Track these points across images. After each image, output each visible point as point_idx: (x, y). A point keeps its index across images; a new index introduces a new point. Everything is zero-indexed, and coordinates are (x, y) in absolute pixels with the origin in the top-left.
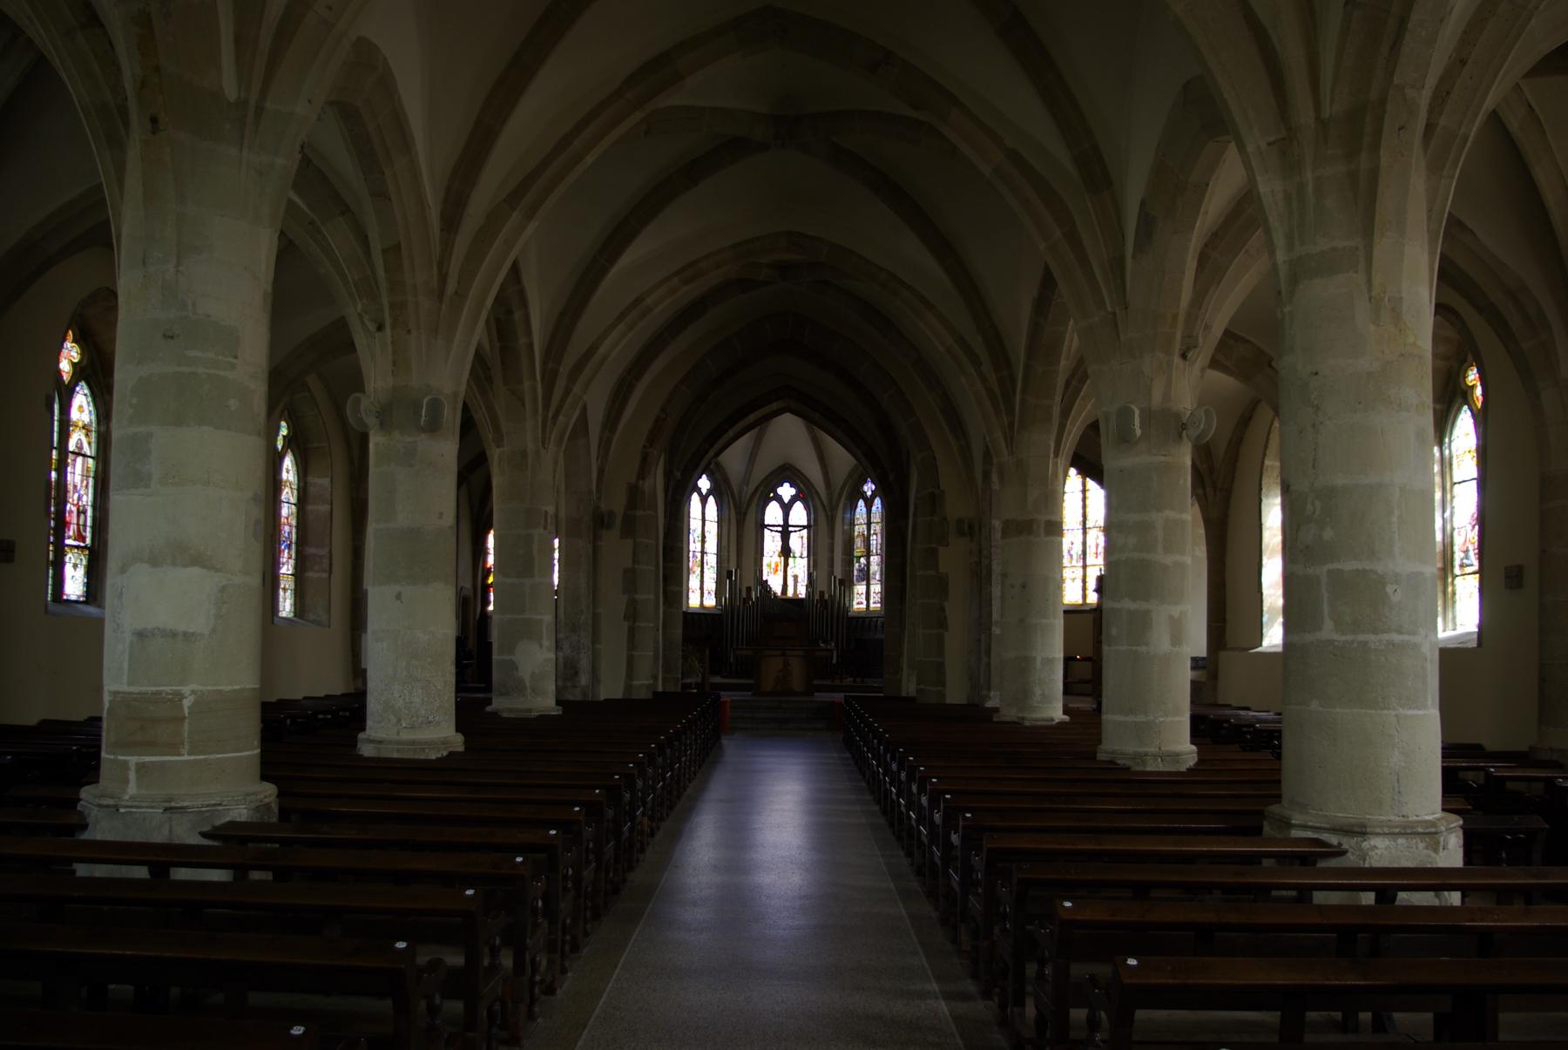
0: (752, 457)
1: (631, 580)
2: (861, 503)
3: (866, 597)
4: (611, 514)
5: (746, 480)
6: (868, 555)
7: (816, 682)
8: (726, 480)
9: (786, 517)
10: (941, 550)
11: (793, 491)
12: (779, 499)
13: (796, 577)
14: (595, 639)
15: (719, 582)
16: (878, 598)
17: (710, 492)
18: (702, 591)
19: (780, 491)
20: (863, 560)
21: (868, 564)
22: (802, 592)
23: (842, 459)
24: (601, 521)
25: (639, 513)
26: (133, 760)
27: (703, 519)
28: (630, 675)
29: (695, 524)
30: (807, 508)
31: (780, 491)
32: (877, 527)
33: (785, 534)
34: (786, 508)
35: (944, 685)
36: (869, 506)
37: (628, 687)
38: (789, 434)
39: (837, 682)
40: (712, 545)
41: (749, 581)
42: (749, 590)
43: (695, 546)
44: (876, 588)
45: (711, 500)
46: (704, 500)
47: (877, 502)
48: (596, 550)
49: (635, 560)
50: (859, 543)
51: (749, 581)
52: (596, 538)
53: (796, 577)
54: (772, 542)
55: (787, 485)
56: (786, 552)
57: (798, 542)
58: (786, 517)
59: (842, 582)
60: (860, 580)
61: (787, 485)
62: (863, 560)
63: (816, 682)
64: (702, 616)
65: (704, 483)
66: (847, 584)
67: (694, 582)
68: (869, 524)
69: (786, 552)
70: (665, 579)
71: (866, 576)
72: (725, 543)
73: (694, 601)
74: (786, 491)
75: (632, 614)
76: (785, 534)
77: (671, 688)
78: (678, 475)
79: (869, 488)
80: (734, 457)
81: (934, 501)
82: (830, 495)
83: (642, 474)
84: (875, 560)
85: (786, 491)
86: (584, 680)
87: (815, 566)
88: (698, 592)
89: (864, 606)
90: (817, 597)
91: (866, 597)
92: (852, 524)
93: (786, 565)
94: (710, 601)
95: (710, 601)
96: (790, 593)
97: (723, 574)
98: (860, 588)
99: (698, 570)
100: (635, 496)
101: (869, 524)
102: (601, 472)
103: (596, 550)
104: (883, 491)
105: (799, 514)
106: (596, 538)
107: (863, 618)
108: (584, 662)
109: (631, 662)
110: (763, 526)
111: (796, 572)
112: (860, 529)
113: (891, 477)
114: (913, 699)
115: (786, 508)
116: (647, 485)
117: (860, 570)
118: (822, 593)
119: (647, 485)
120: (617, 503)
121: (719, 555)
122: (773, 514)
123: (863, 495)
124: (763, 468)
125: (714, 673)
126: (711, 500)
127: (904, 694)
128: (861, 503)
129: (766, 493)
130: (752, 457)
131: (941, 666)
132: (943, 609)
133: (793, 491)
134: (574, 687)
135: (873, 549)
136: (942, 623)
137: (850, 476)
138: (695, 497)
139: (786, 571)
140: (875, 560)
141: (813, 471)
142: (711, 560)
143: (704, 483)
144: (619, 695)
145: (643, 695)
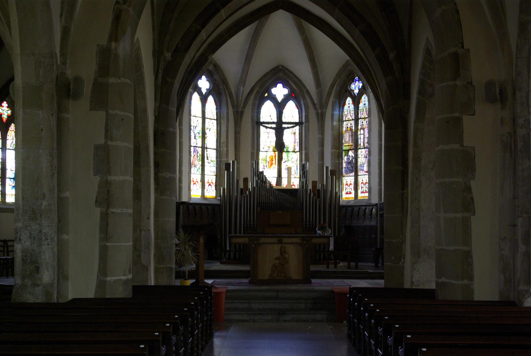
0: (248, 59)
1: (103, 159)
2: (349, 100)
3: (356, 187)
4: (78, 81)
5: (243, 81)
6: (356, 149)
7: (313, 268)
8: (225, 82)
9: (279, 113)
10: (467, 120)
11: (286, 91)
12: (273, 99)
13: (289, 170)
14: (61, 226)
15: (219, 175)
16: (366, 188)
17: (210, 92)
18: (201, 183)
19: (274, 91)
20: (351, 153)
21: (356, 157)
22: (296, 183)
23: (332, 55)
24: (66, 90)
25: (112, 80)
26: (228, 235)
27: (202, 115)
28: (103, 270)
29: (196, 122)
30: (299, 106)
31: (274, 91)
32: (363, 123)
33: (279, 129)
34: (280, 107)
35: (471, 278)
36: (356, 101)
37: (101, 284)
38: (281, 36)
39: (332, 268)
40: (211, 141)
41: (246, 172)
42: (246, 180)
43: (196, 142)
44: (363, 178)
45: (211, 99)
46: (204, 99)
47: (364, 99)
48: (60, 122)
49: (108, 135)
50: (347, 139)
51: (246, 172)
52: (61, 109)
53: (289, 170)
54: (267, 138)
55: (280, 86)
56: (280, 147)
57: (291, 138)
58: (279, 113)
59: (333, 173)
60: (349, 171)
61: (280, 86)
62: (351, 153)
63: (313, 268)
64: (202, 208)
65: (204, 84)
66: (336, 174)
67: (195, 175)
68: (356, 120)
69: (280, 147)
70: (156, 165)
71: (354, 168)
72: (223, 139)
73: (196, 193)
74: (280, 91)
75: (105, 199)
76: (279, 129)
77: (165, 281)
78: (168, 55)
79: (356, 87)
80: (230, 55)
81: (458, 62)
82: (320, 94)
83: (115, 35)
84: (362, 153)
85: (280, 91)
86: (47, 276)
87: (307, 159)
88: (199, 184)
89: (352, 196)
90: (310, 187)
91: (356, 187)
92: (341, 121)
93: (280, 159)
94: (211, 193)
95: (211, 193)
96: (284, 184)
97: (223, 167)
98: (348, 179)
99: (199, 164)
100: (106, 60)
101: (356, 120)
102: (65, 32)
103: (60, 122)
104: (371, 85)
105: (291, 113)
106: (61, 109)
107: (352, 207)
108: (47, 255)
109: (104, 253)
110: (259, 124)
111: (289, 164)
112: (348, 124)
113: (392, 56)
114: (429, 294)
115: (280, 107)
116: (123, 48)
117: (349, 163)
118: (314, 183)
119: (123, 48)
120: (86, 69)
121: (218, 150)
122: (268, 112)
123: (350, 93)
124: (260, 67)
125: (211, 258)
126: (211, 99)
127: (407, 285)
128: (349, 100)
129: (262, 94)
130: (248, 59)
131: (467, 256)
132: (468, 189)
133: (286, 91)
134: (35, 285)
135: (361, 142)
136: (468, 206)
137: (339, 75)
138: (196, 98)
139: (281, 165)
140: (362, 153)
141: (304, 71)
142: (212, 154)
143: (204, 84)
144: (91, 294)
145: (120, 292)
